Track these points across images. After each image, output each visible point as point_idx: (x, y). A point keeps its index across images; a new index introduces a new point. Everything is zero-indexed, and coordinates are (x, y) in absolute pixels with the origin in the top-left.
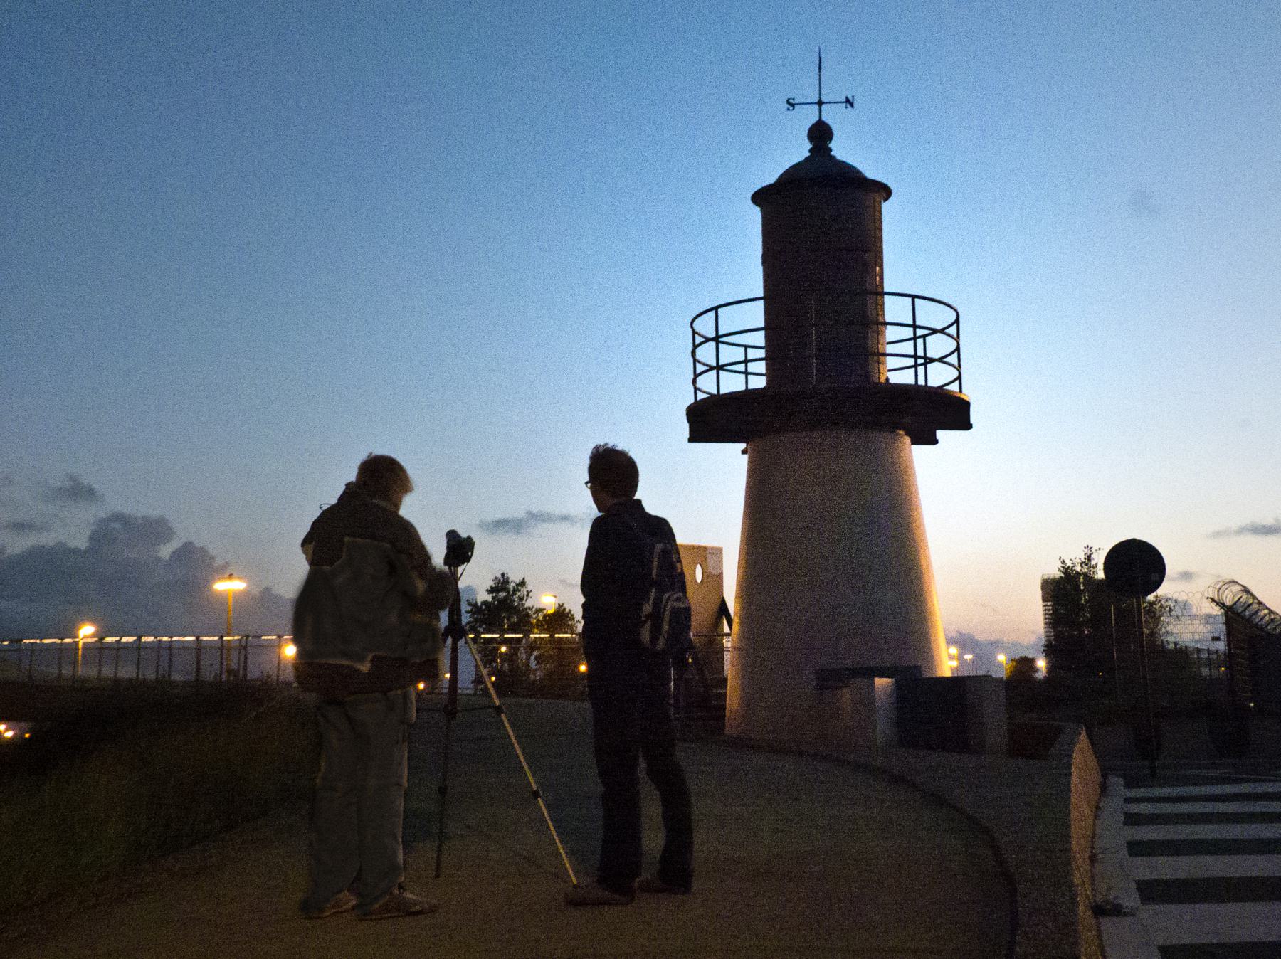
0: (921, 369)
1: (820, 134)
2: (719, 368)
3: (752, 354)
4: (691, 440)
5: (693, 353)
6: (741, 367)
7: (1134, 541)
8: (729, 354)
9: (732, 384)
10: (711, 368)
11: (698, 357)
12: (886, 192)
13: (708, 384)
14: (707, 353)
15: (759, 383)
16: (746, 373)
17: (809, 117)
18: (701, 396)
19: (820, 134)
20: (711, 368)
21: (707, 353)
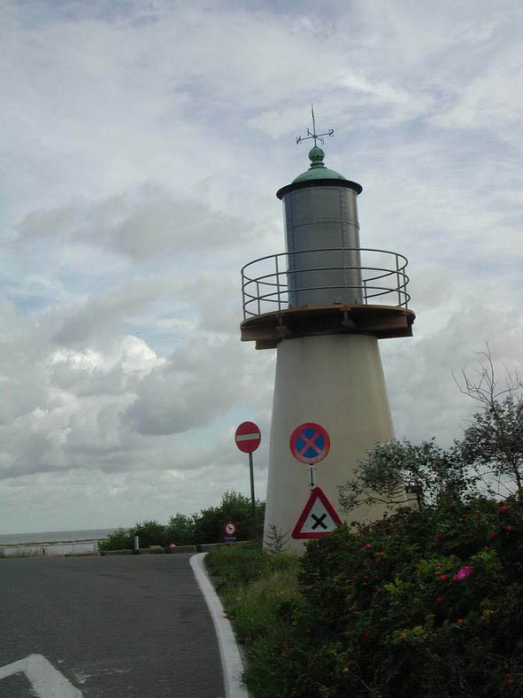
0: (402, 284)
1: (316, 157)
2: (259, 298)
3: (282, 289)
4: (243, 340)
5: (242, 272)
6: (275, 297)
7: (252, 423)
8: (264, 290)
9: (268, 307)
10: (255, 299)
11: (245, 275)
12: (357, 189)
13: (253, 308)
14: (251, 289)
15: (285, 307)
16: (278, 285)
17: (309, 145)
18: (248, 316)
19: (316, 157)
20: (255, 299)
21: (251, 289)
